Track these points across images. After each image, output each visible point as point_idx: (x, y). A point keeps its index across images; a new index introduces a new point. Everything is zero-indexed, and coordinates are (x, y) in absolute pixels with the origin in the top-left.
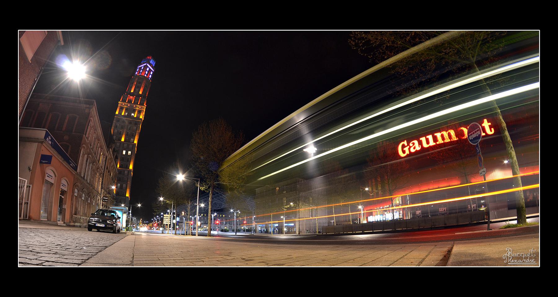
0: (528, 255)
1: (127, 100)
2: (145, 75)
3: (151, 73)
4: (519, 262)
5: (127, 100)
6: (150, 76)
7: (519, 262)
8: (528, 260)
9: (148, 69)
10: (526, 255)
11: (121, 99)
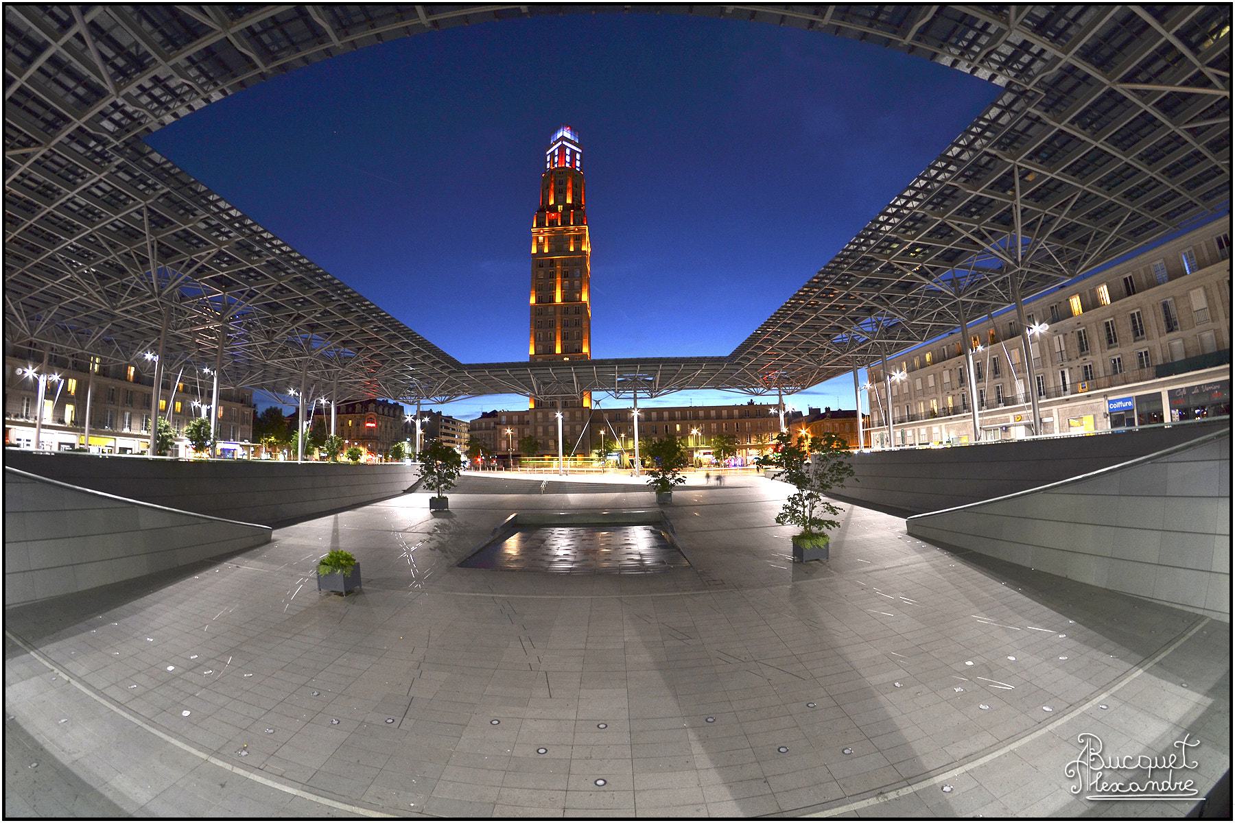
0: (1167, 764)
1: (547, 221)
2: (568, 165)
3: (578, 156)
4: (1130, 792)
5: (547, 221)
6: (578, 164)
7: (1130, 792)
8: (1166, 785)
9: (568, 151)
10: (1160, 763)
11: (572, 220)
